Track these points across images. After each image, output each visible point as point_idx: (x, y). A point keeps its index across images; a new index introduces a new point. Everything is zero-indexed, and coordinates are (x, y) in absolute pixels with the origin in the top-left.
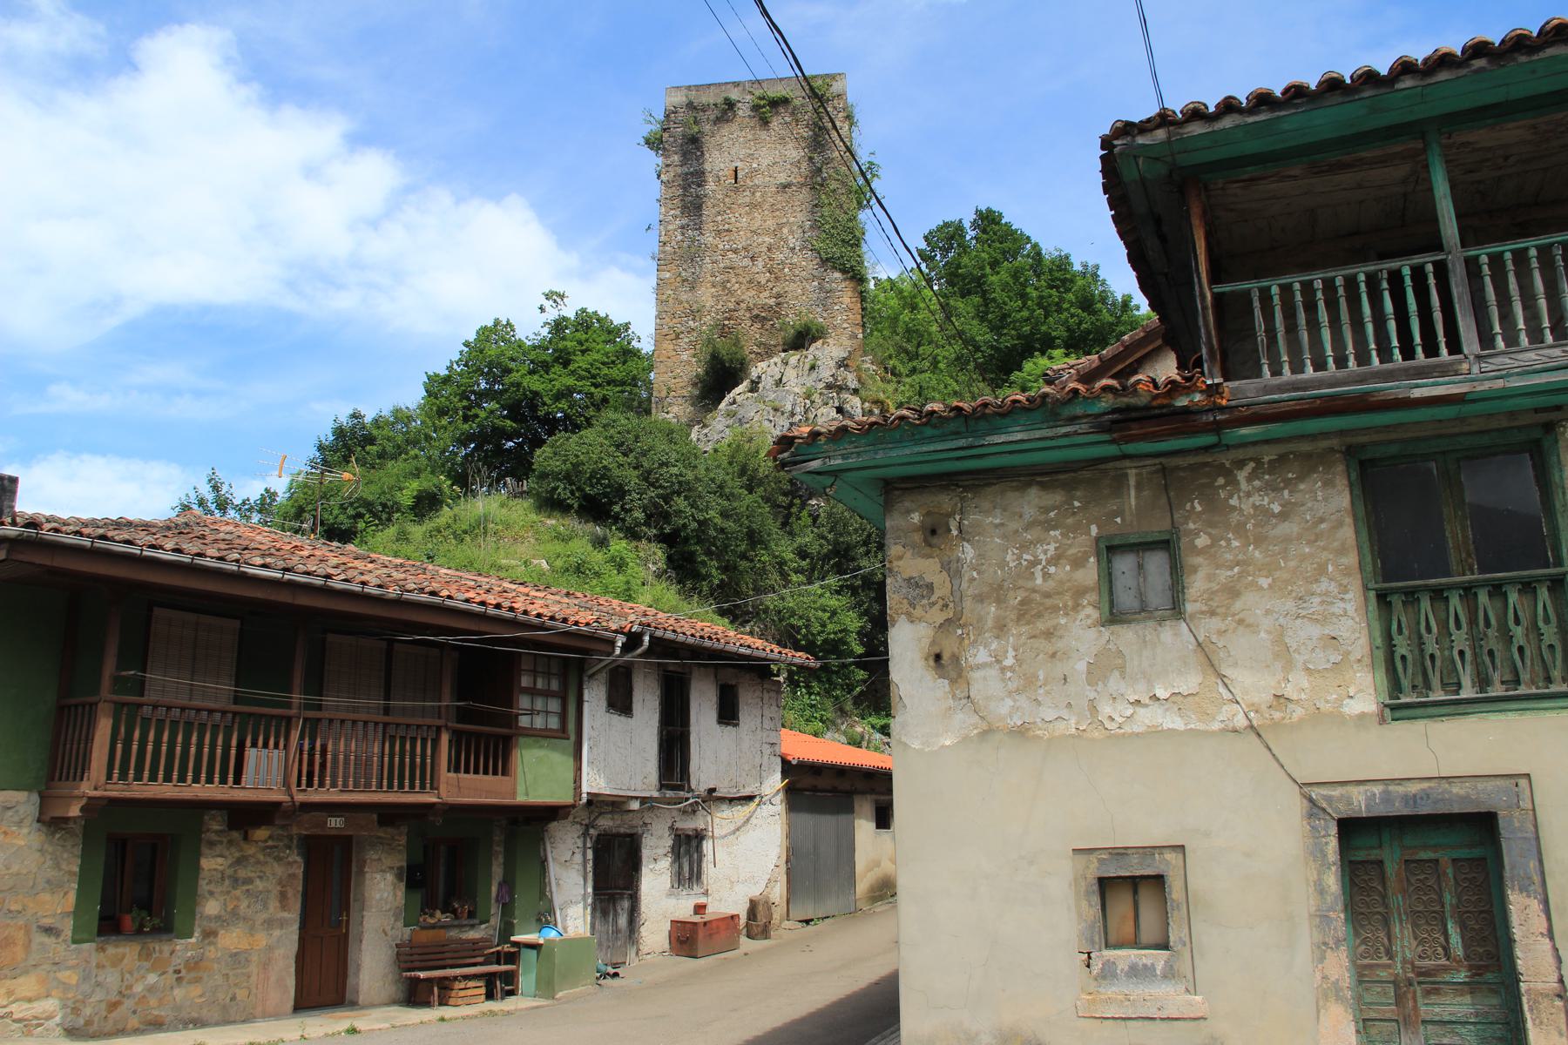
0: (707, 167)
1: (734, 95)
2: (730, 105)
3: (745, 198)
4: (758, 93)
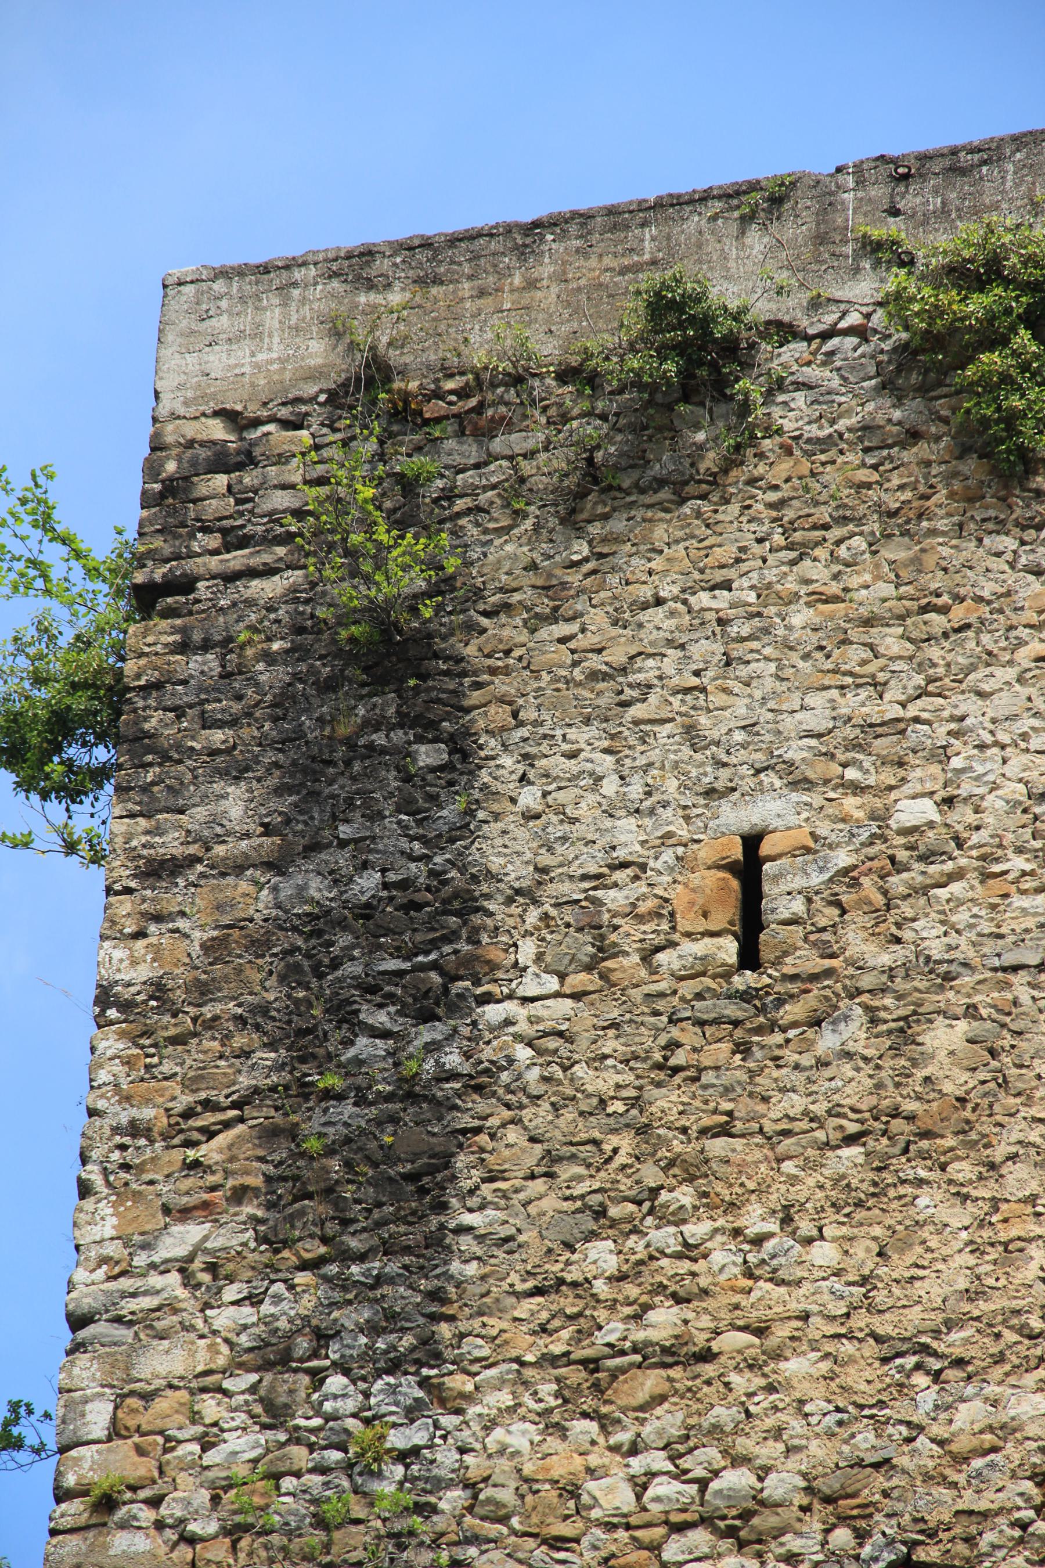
0: (504, 852)
1: (741, 278)
2: (701, 360)
3: (838, 1064)
4: (939, 245)
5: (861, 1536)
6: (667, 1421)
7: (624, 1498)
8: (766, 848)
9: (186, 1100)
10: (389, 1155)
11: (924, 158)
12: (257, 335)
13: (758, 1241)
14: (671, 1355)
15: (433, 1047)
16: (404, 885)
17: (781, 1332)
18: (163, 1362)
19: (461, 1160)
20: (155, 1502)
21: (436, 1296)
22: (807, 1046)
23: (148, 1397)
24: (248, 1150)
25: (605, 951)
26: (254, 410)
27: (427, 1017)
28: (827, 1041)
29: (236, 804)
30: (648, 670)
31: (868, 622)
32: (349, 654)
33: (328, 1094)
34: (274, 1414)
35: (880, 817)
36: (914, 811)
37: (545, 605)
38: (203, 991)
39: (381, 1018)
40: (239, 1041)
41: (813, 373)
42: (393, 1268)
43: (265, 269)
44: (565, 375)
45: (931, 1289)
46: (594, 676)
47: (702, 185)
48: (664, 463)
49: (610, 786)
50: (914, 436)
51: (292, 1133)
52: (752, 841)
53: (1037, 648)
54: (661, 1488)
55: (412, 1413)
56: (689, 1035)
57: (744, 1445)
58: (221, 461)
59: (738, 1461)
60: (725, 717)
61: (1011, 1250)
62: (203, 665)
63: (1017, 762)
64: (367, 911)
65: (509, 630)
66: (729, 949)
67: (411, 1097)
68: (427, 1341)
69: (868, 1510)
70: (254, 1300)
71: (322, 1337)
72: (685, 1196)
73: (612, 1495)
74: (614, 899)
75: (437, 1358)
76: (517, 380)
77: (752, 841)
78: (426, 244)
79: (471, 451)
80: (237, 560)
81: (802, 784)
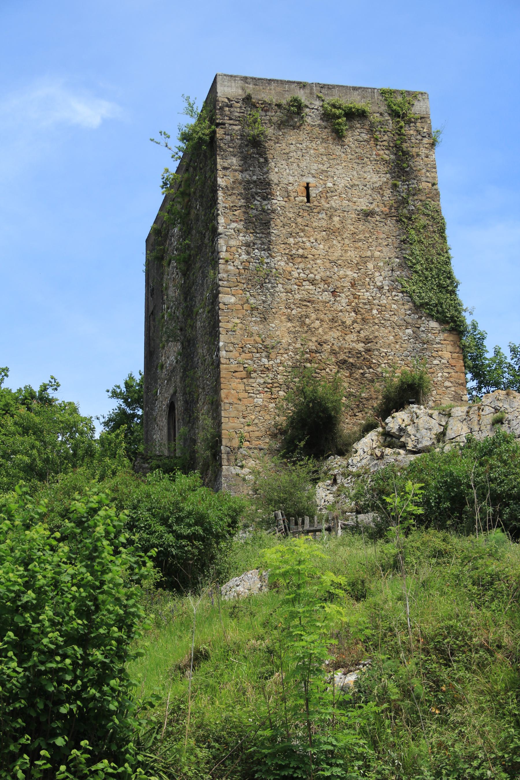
1: (302, 96)
3: (320, 220)
5: (329, 286)
6: (302, 266)
7: (297, 275)
8: (310, 185)
9: (231, 205)
10: (261, 219)
11: (324, 85)
12: (231, 87)
13: (312, 243)
14: (302, 256)
15: (266, 205)
16: (260, 179)
17: (317, 256)
18: (232, 243)
19: (272, 222)
20: (233, 262)
21: (269, 241)
22: (318, 216)
23: (231, 247)
24: (242, 214)
25: (288, 196)
26: (232, 99)
27: (264, 200)
28: (320, 216)
29: (234, 160)
30: (291, 154)
31: (321, 155)
32: (249, 141)
33: (252, 208)
34: (248, 253)
35: (325, 184)
36: (330, 185)
37: (276, 141)
38: (233, 189)
39: (259, 199)
40: (239, 197)
41: (311, 114)
42: (263, 236)
43: (231, 76)
44: (276, 105)
45: (336, 254)
46: (284, 153)
47: (294, 80)
48: (291, 123)
49: (288, 171)
50: (326, 128)
51: (248, 213)
52: (308, 184)
53: (3, 546)
54: (302, 275)
55: (267, 257)
56: (302, 211)
57: (312, 271)
58: (227, 106)
59: (311, 273)
60: (303, 164)
61: (346, 251)
62: (228, 138)
63: (343, 181)
64: (255, 182)
65: (272, 143)
66: (305, 199)
67: (264, 211)
68: (269, 247)
69: (329, 283)
70: (244, 236)
71: (254, 244)
72: (302, 234)
73: (295, 274)
74: (290, 188)
75: (270, 250)
76: (270, 104)
77: (308, 184)
78: (255, 79)
79: (263, 114)
80: (231, 122)
81: (314, 177)
